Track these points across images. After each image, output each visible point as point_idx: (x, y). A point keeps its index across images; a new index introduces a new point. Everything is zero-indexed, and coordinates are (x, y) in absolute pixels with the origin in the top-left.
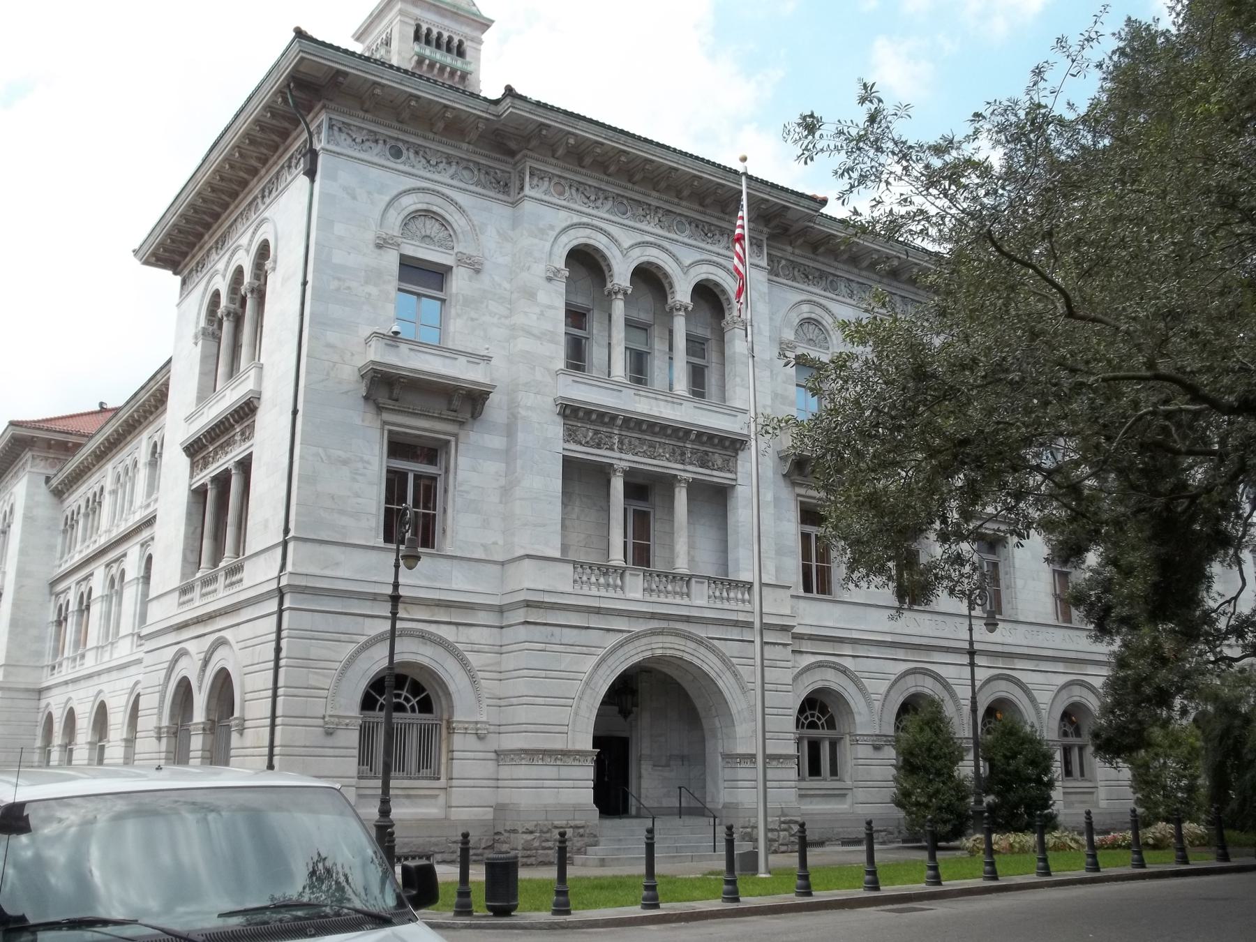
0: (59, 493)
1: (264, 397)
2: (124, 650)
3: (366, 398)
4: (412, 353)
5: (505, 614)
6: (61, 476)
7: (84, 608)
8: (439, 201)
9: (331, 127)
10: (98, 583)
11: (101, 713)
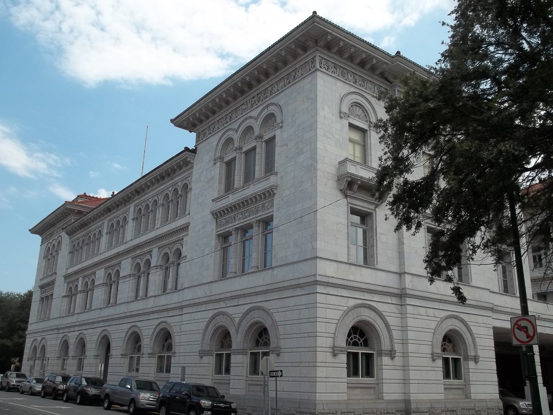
5: (403, 298)
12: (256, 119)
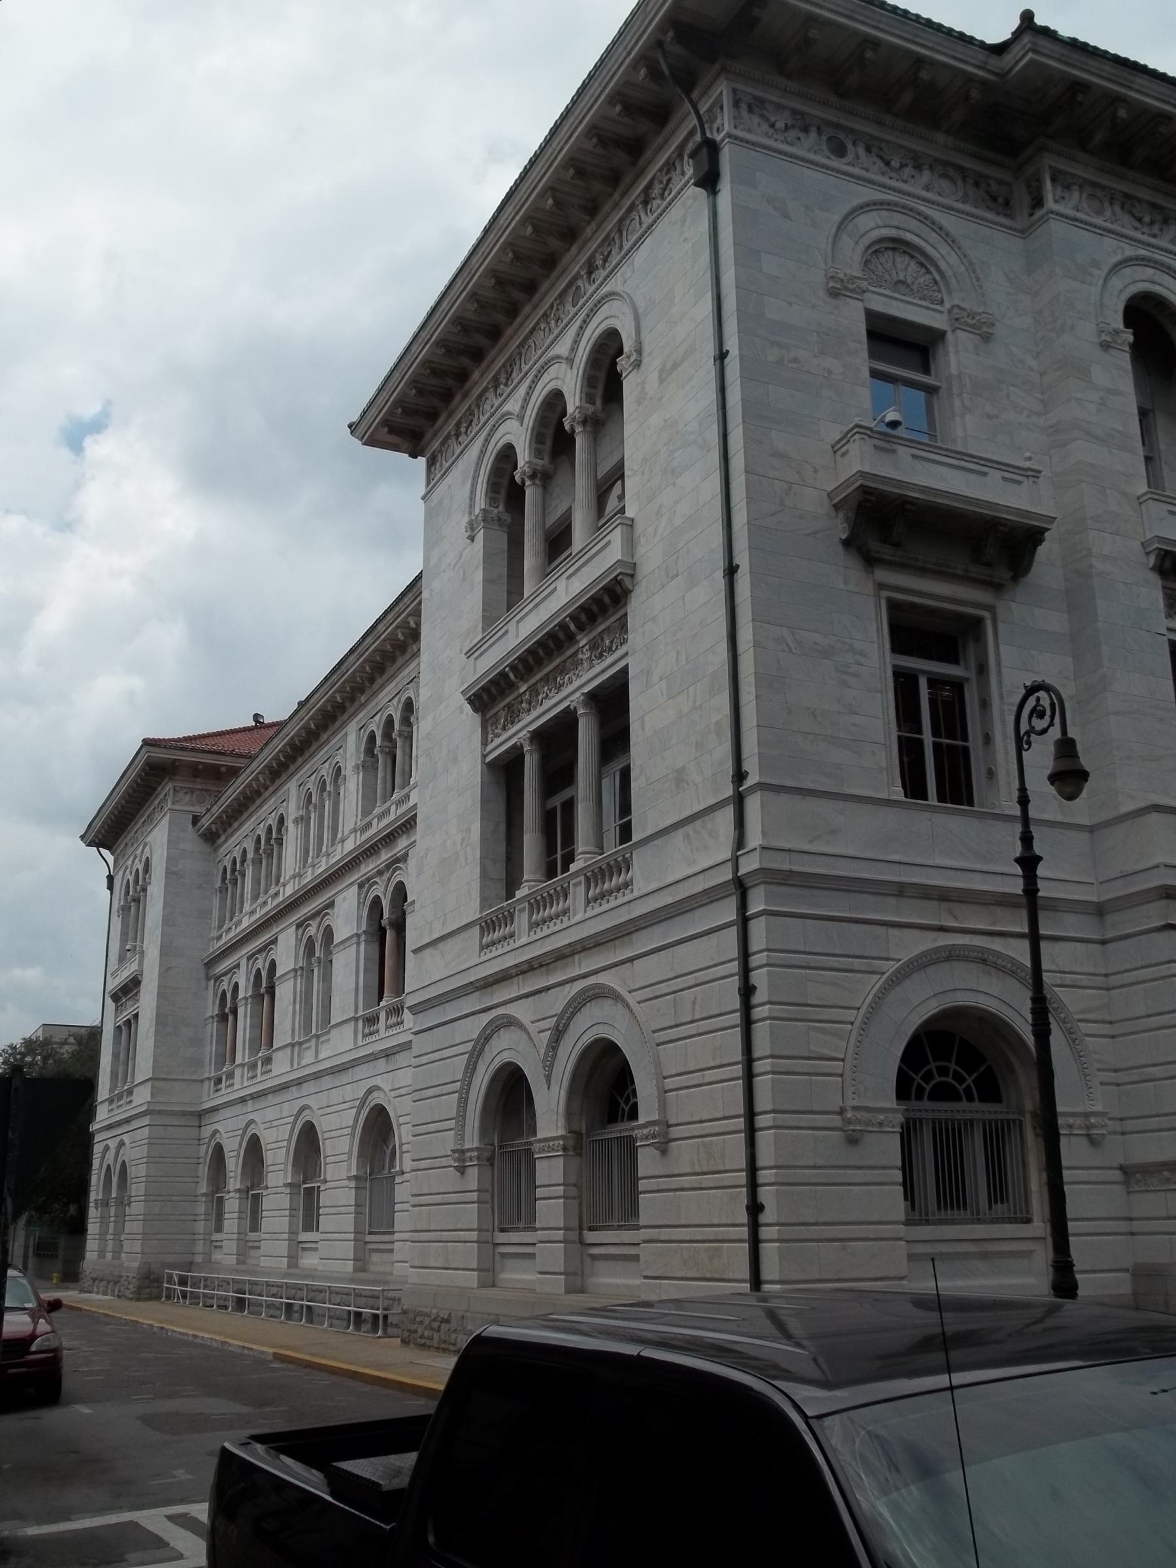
0: (211, 838)
1: (644, 570)
2: (342, 1043)
3: (847, 543)
4: (918, 464)
5: (1109, 919)
6: (216, 810)
7: (265, 990)
8: (914, 224)
9: (736, 104)
10: (286, 951)
11: (308, 1142)
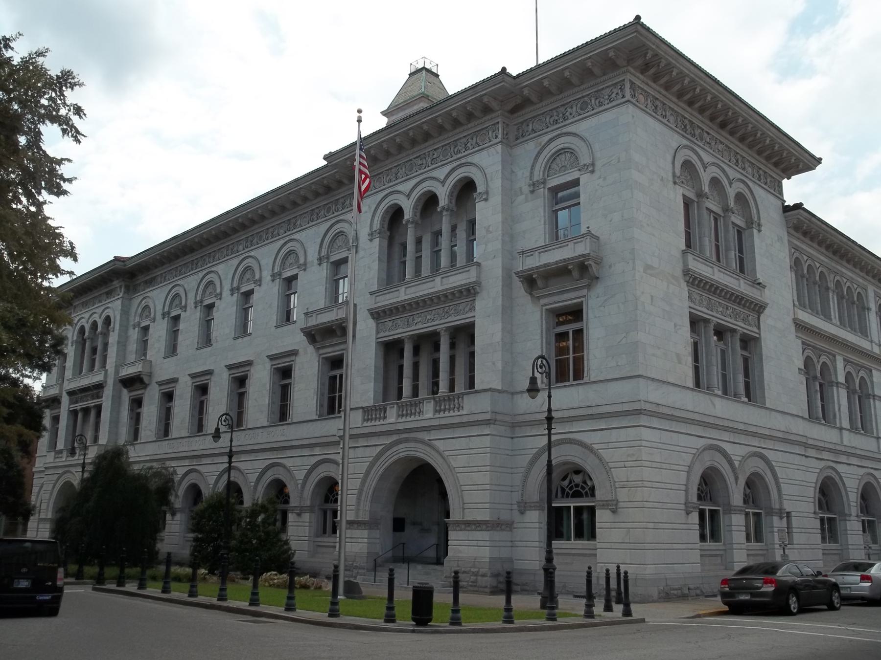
12: (443, 183)
